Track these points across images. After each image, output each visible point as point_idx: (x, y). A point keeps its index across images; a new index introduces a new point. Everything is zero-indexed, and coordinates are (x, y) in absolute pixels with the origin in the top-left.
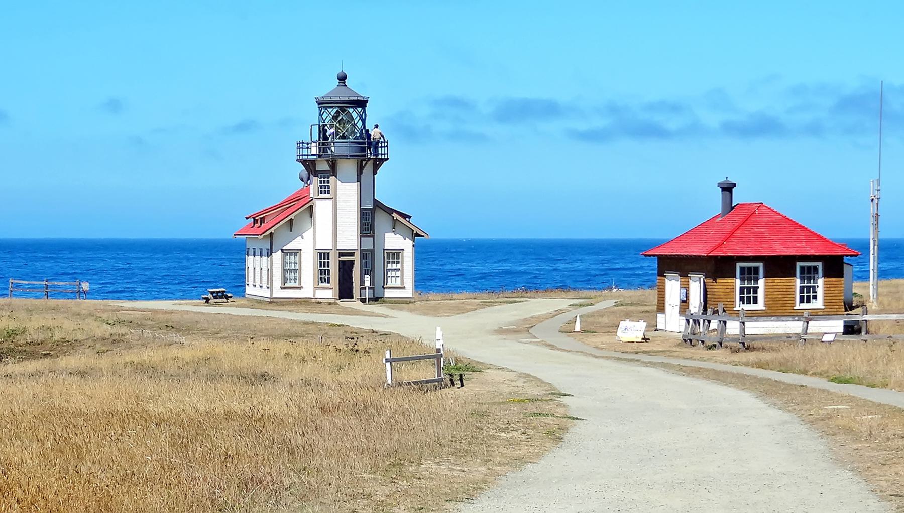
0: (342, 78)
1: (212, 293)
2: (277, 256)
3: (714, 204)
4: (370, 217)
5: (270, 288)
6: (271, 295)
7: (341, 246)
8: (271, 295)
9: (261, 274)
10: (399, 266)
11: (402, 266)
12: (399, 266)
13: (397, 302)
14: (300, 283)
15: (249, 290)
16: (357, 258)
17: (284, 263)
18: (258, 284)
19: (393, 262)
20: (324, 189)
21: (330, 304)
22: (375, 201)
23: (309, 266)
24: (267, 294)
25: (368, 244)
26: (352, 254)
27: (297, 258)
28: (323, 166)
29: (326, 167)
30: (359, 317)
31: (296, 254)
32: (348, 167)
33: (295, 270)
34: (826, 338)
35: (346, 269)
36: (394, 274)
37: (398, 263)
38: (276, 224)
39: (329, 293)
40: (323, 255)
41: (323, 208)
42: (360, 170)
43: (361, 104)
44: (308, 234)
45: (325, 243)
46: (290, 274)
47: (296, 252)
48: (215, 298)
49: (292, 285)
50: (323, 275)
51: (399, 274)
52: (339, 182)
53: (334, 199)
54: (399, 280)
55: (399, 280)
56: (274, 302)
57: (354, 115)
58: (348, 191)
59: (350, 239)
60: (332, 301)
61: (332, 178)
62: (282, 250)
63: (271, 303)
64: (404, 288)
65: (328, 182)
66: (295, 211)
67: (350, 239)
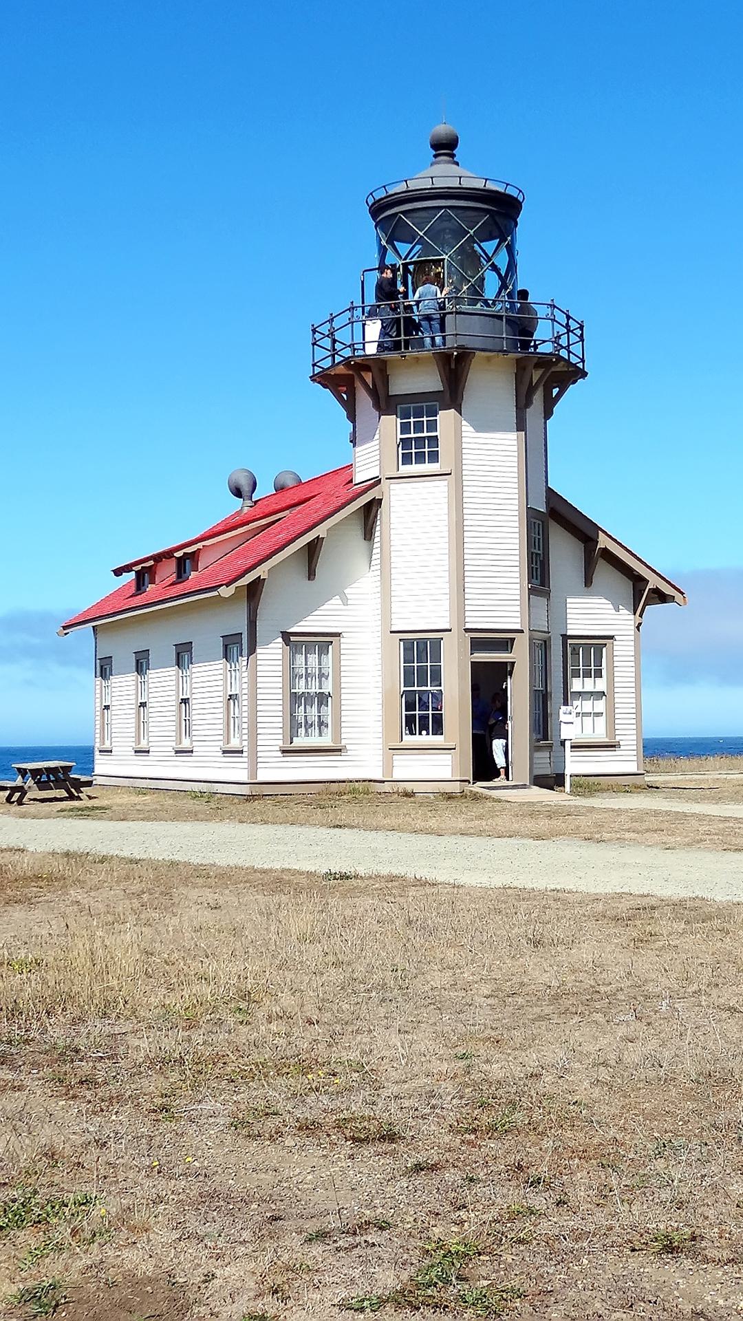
1: (35, 773)
2: (271, 653)
4: (560, 534)
6: (253, 771)
7: (478, 620)
8: (253, 771)
10: (601, 684)
11: (611, 683)
12: (601, 684)
14: (337, 734)
16: (520, 656)
17: (292, 676)
19: (587, 674)
20: (418, 449)
21: (449, 797)
22: (551, 493)
23: (366, 685)
24: (237, 771)
26: (506, 644)
27: (328, 660)
28: (418, 379)
29: (429, 381)
31: (323, 648)
32: (491, 384)
33: (323, 699)
34: (498, 745)
36: (587, 706)
37: (599, 674)
39: (439, 763)
40: (420, 652)
41: (413, 507)
42: (523, 404)
43: (500, 212)
44: (363, 586)
45: (427, 610)
46: (308, 706)
47: (324, 642)
48: (42, 786)
49: (314, 741)
50: (420, 715)
51: (600, 706)
52: (467, 428)
53: (454, 476)
54: (601, 721)
55: (601, 721)
56: (260, 799)
58: (486, 454)
59: (501, 603)
60: (455, 788)
61: (445, 417)
62: (286, 636)
63: (250, 798)
64: (612, 746)
65: (432, 426)
66: (307, 526)
67: (501, 603)
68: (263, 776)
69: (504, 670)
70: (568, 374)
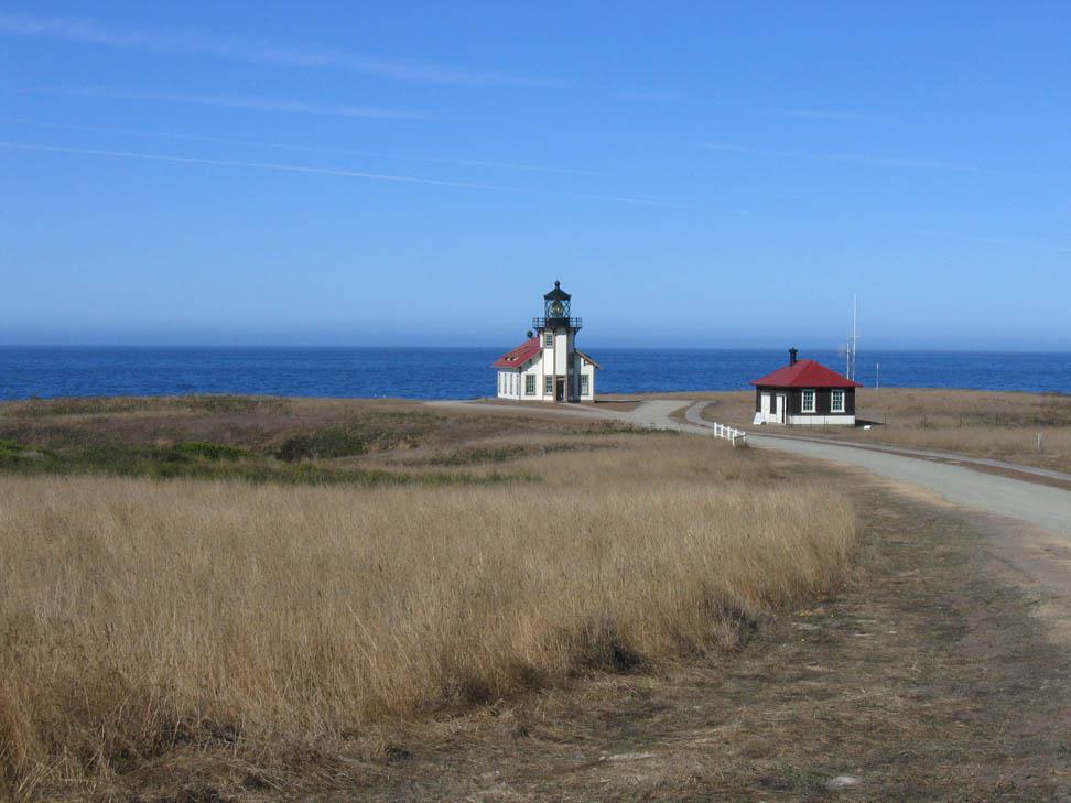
0: (558, 284)
3: (554, 287)
5: (518, 393)
7: (558, 373)
9: (509, 386)
13: (587, 403)
15: (501, 395)
16: (566, 379)
18: (508, 390)
24: (517, 398)
25: (571, 372)
30: (570, 411)
35: (560, 385)
38: (525, 356)
39: (550, 398)
41: (548, 353)
45: (549, 371)
46: (530, 388)
50: (547, 388)
57: (564, 305)
67: (562, 370)
68: (522, 398)
69: (562, 382)
70: (576, 330)
